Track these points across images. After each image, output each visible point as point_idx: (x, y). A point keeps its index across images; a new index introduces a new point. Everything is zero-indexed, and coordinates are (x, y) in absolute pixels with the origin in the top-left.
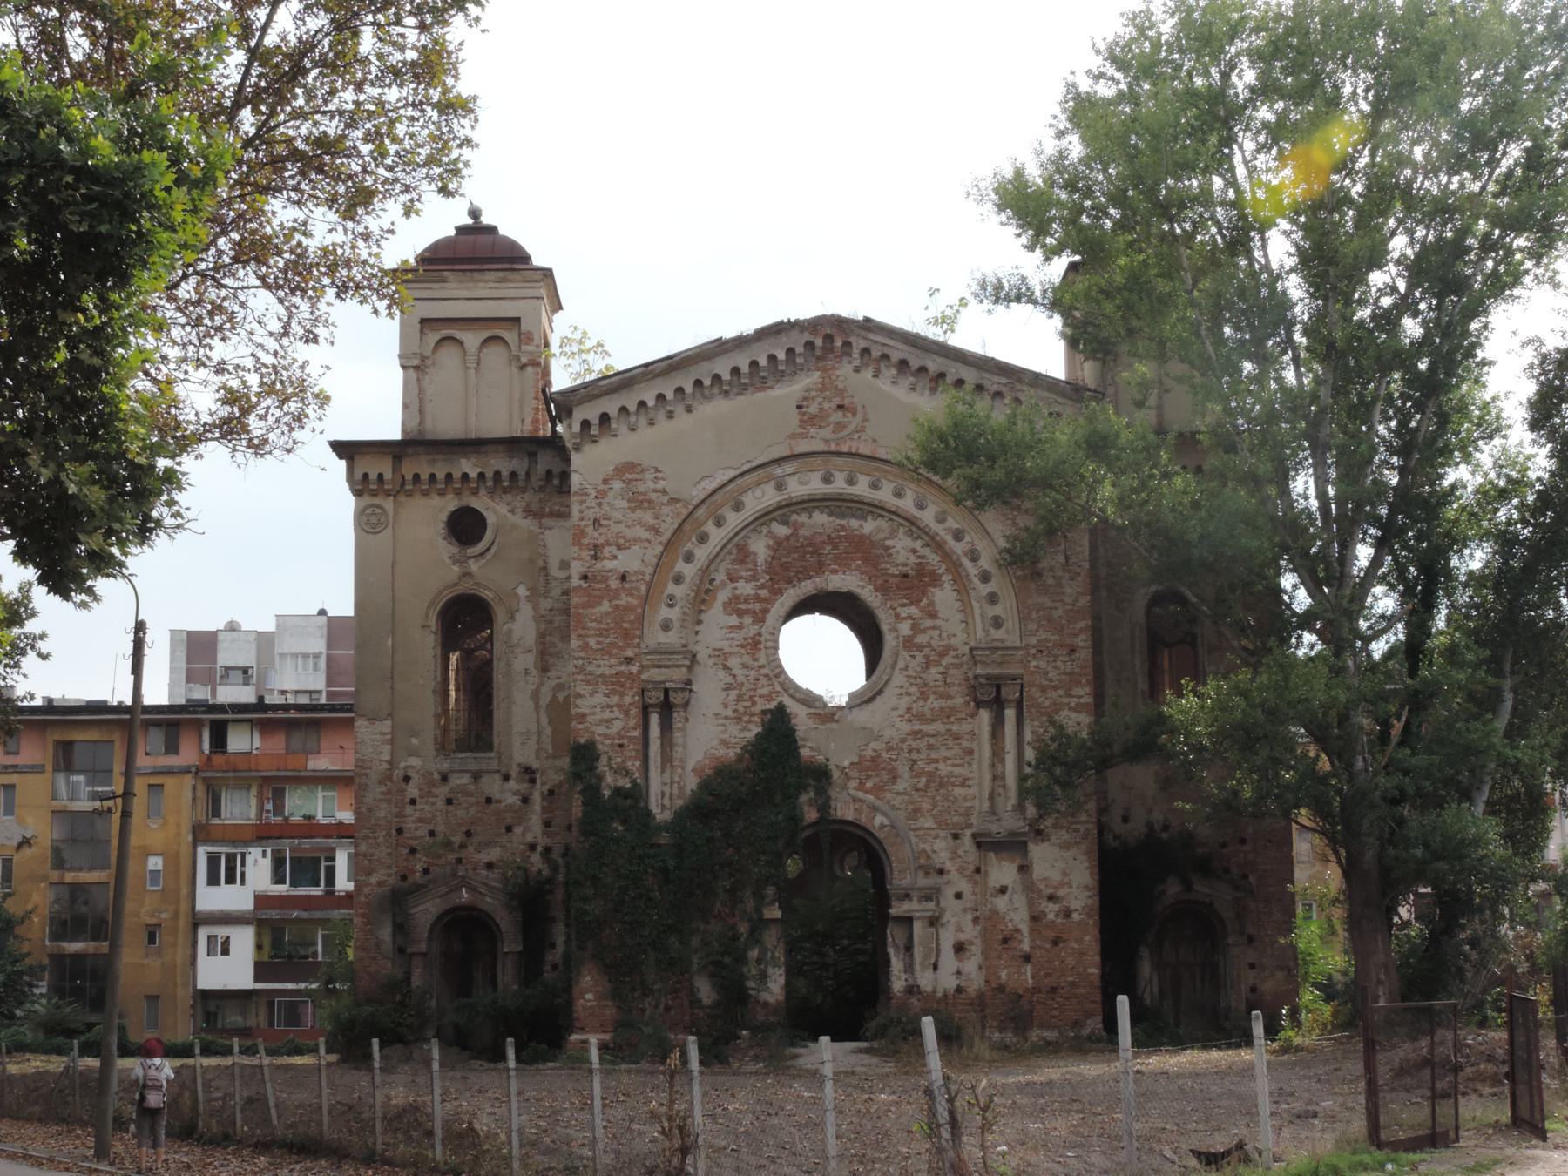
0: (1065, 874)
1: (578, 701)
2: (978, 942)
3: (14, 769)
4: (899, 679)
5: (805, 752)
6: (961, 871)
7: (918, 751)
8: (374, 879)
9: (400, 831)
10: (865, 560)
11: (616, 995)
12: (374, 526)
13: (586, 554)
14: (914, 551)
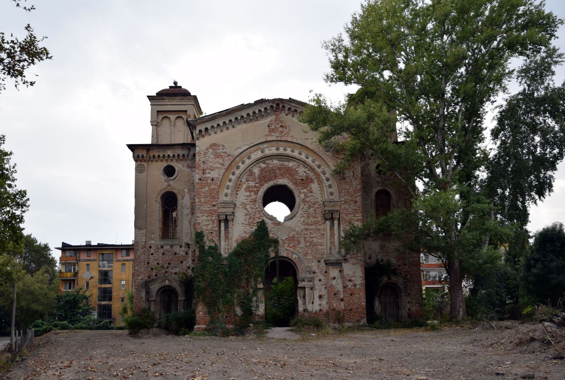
0: (354, 273)
1: (198, 219)
2: (326, 295)
3: (90, 260)
4: (300, 212)
5: (271, 235)
6: (321, 272)
7: (307, 234)
8: (140, 278)
9: (148, 263)
10: (290, 175)
11: (209, 313)
12: (141, 171)
13: (201, 172)
14: (305, 172)
